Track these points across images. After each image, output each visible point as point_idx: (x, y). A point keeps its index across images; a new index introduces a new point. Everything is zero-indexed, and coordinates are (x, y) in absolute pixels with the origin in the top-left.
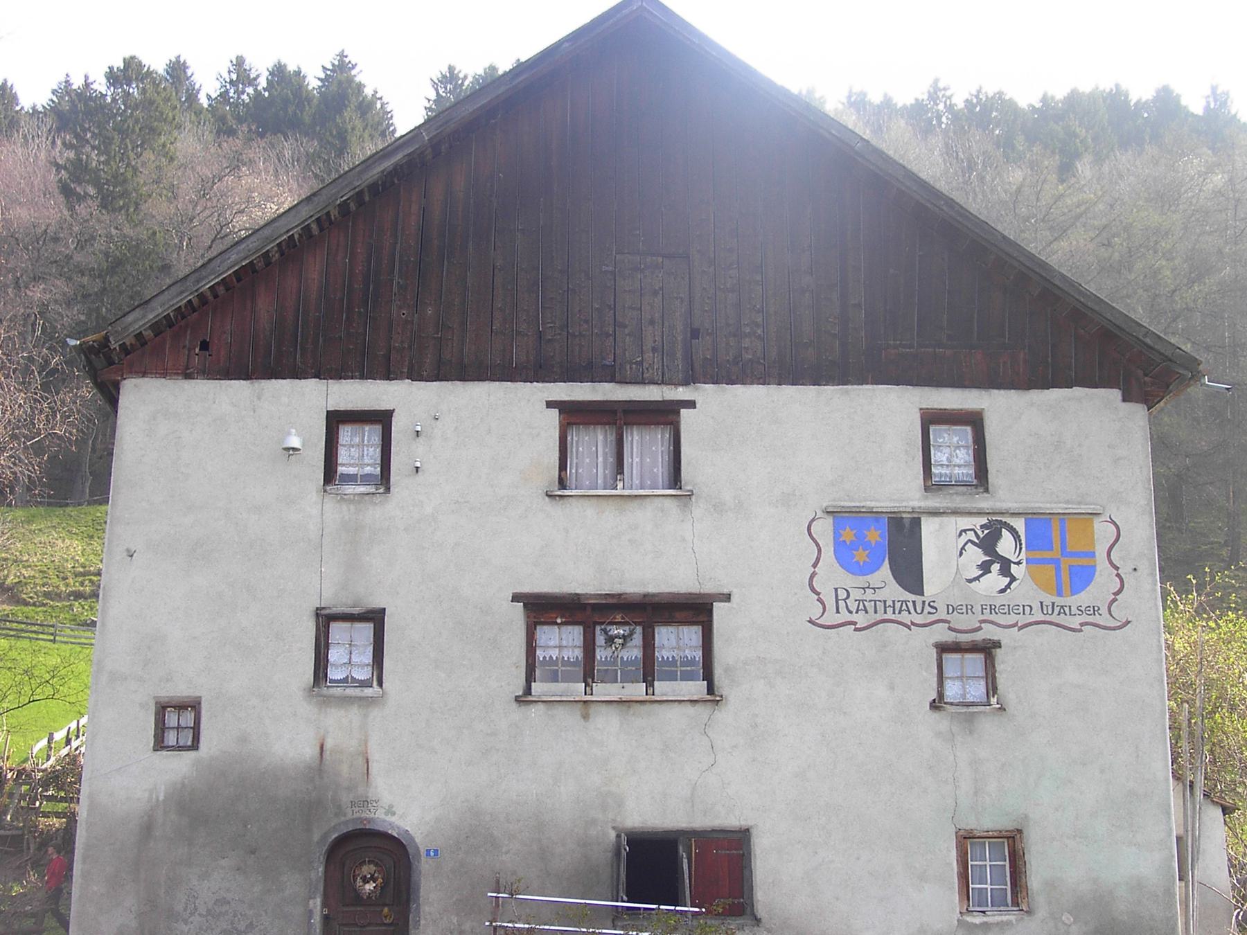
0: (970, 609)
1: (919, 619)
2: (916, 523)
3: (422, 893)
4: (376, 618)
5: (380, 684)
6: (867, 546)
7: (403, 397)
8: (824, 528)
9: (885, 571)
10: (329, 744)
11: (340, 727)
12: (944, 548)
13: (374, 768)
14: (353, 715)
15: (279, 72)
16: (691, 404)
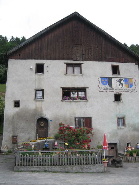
0: (118, 89)
1: (112, 91)
2: (111, 79)
3: (50, 126)
4: (42, 90)
5: (43, 99)
6: (105, 82)
7: (46, 63)
8: (100, 79)
9: (108, 85)
10: (37, 106)
11: (38, 104)
12: (115, 82)
13: (43, 110)
14: (40, 103)
15: (17, 38)
16: (83, 63)
